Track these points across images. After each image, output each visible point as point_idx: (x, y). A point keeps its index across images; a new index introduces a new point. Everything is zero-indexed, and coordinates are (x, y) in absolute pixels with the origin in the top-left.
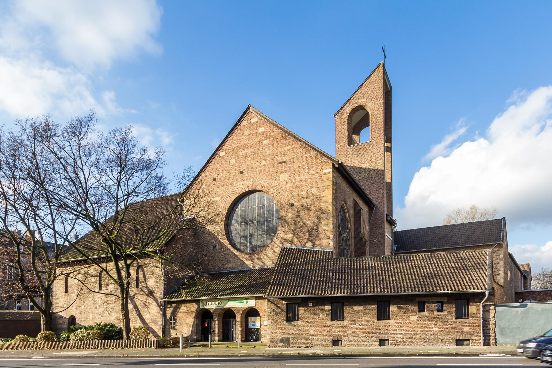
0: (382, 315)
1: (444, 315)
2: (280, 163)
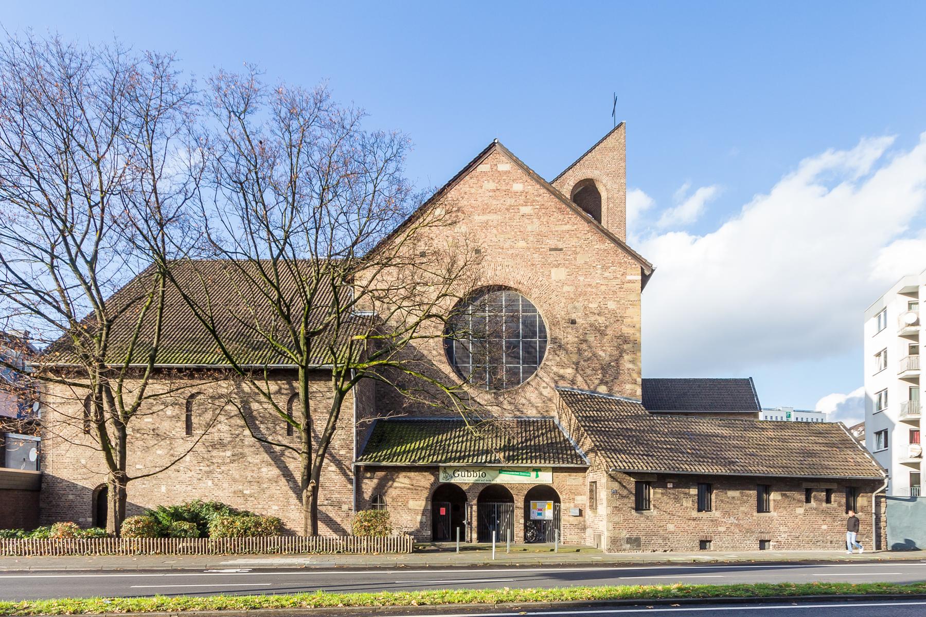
1: (833, 508)
2: (551, 250)
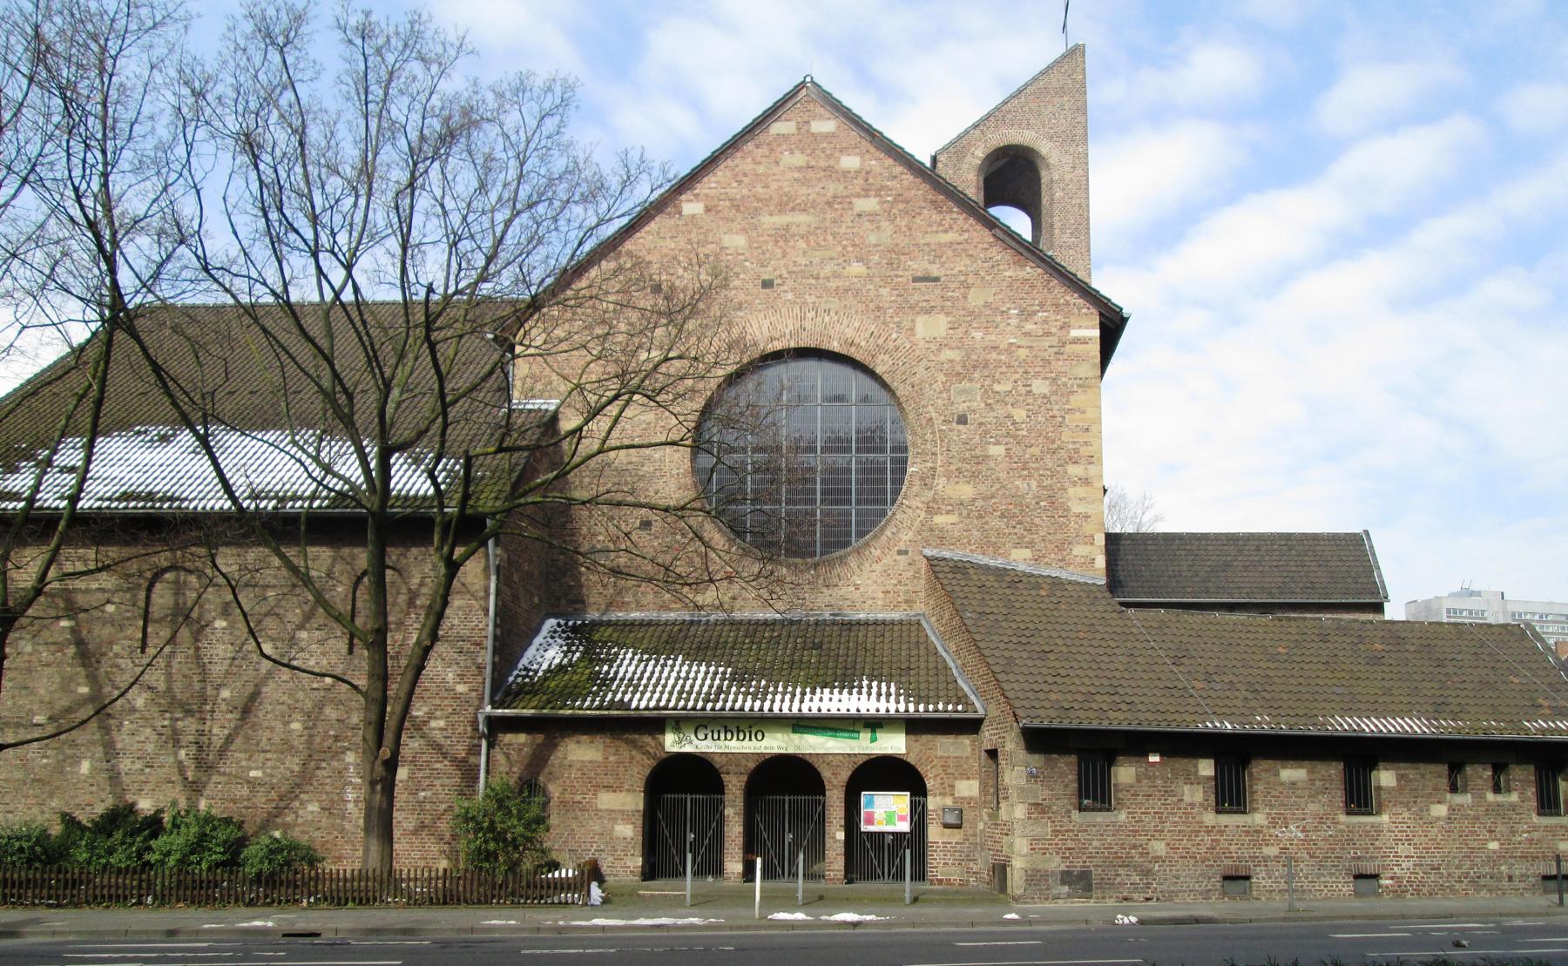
0: (1359, 798)
2: (916, 280)
